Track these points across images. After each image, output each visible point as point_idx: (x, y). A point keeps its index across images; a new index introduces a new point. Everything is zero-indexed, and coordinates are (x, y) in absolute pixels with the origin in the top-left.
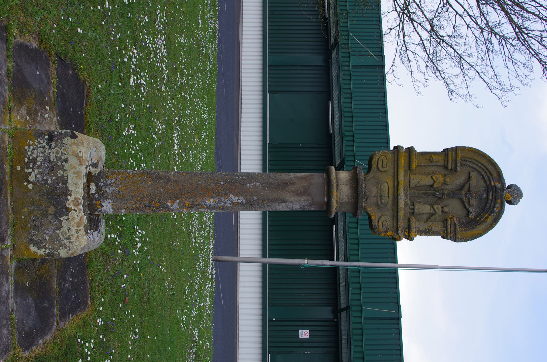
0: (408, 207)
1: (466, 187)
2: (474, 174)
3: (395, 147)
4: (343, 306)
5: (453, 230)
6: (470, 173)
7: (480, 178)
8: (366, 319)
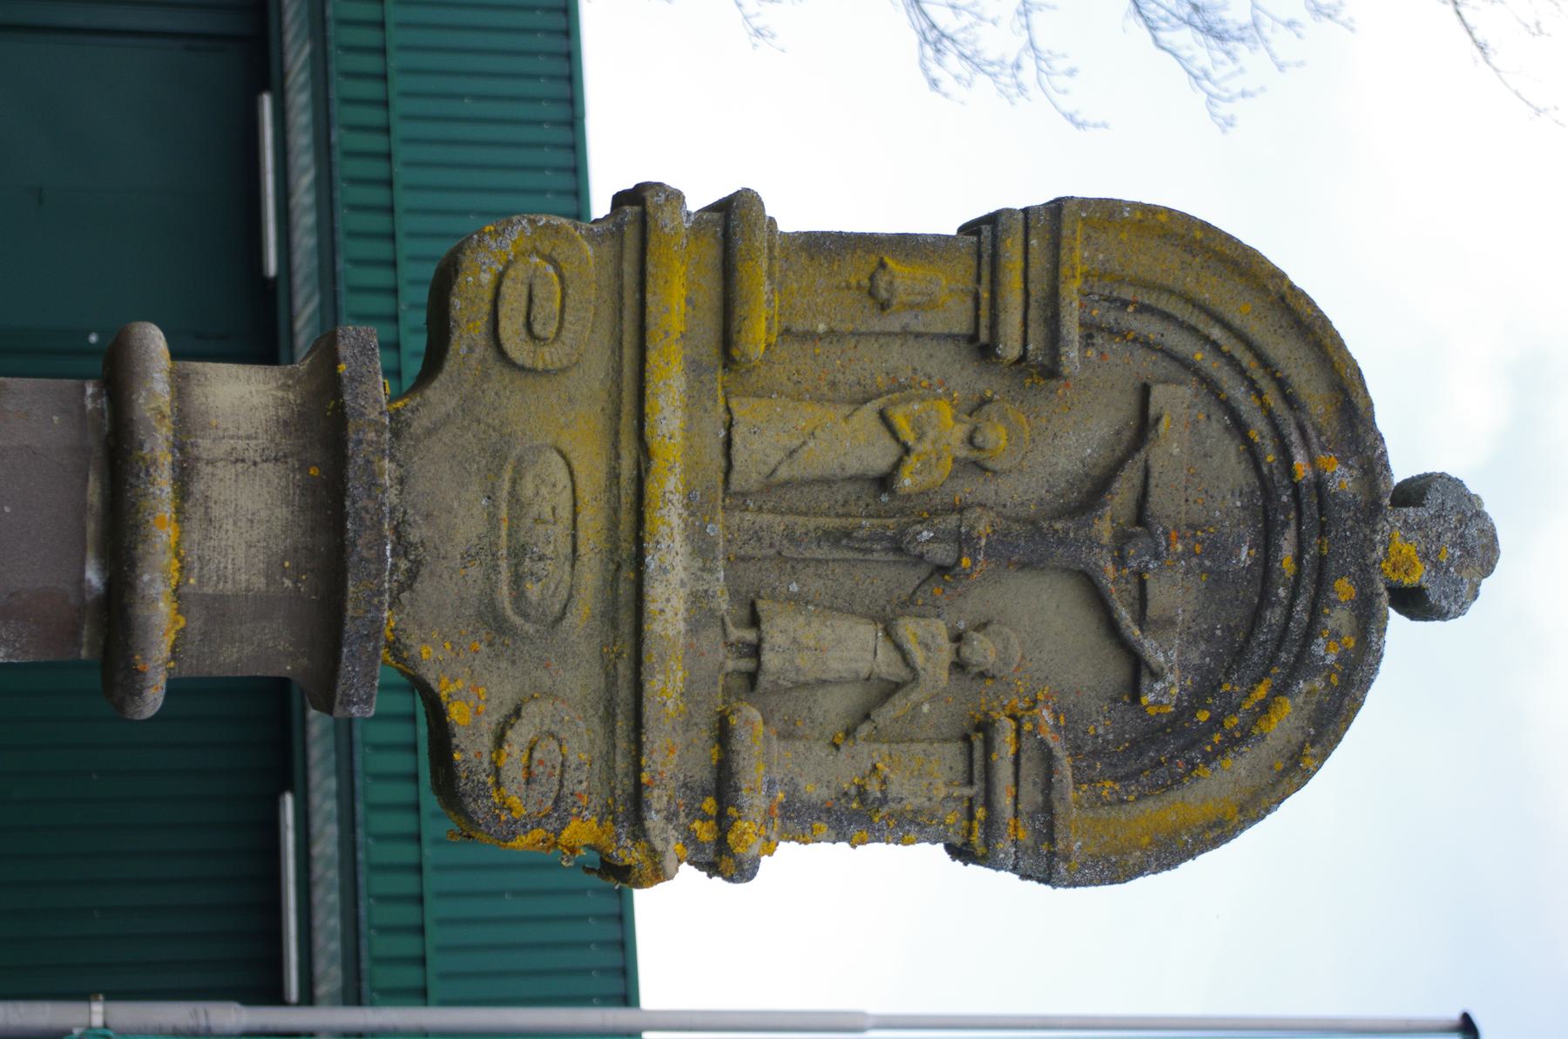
0: (714, 633)
1: (1122, 494)
5: (1031, 795)
6: (1145, 391)
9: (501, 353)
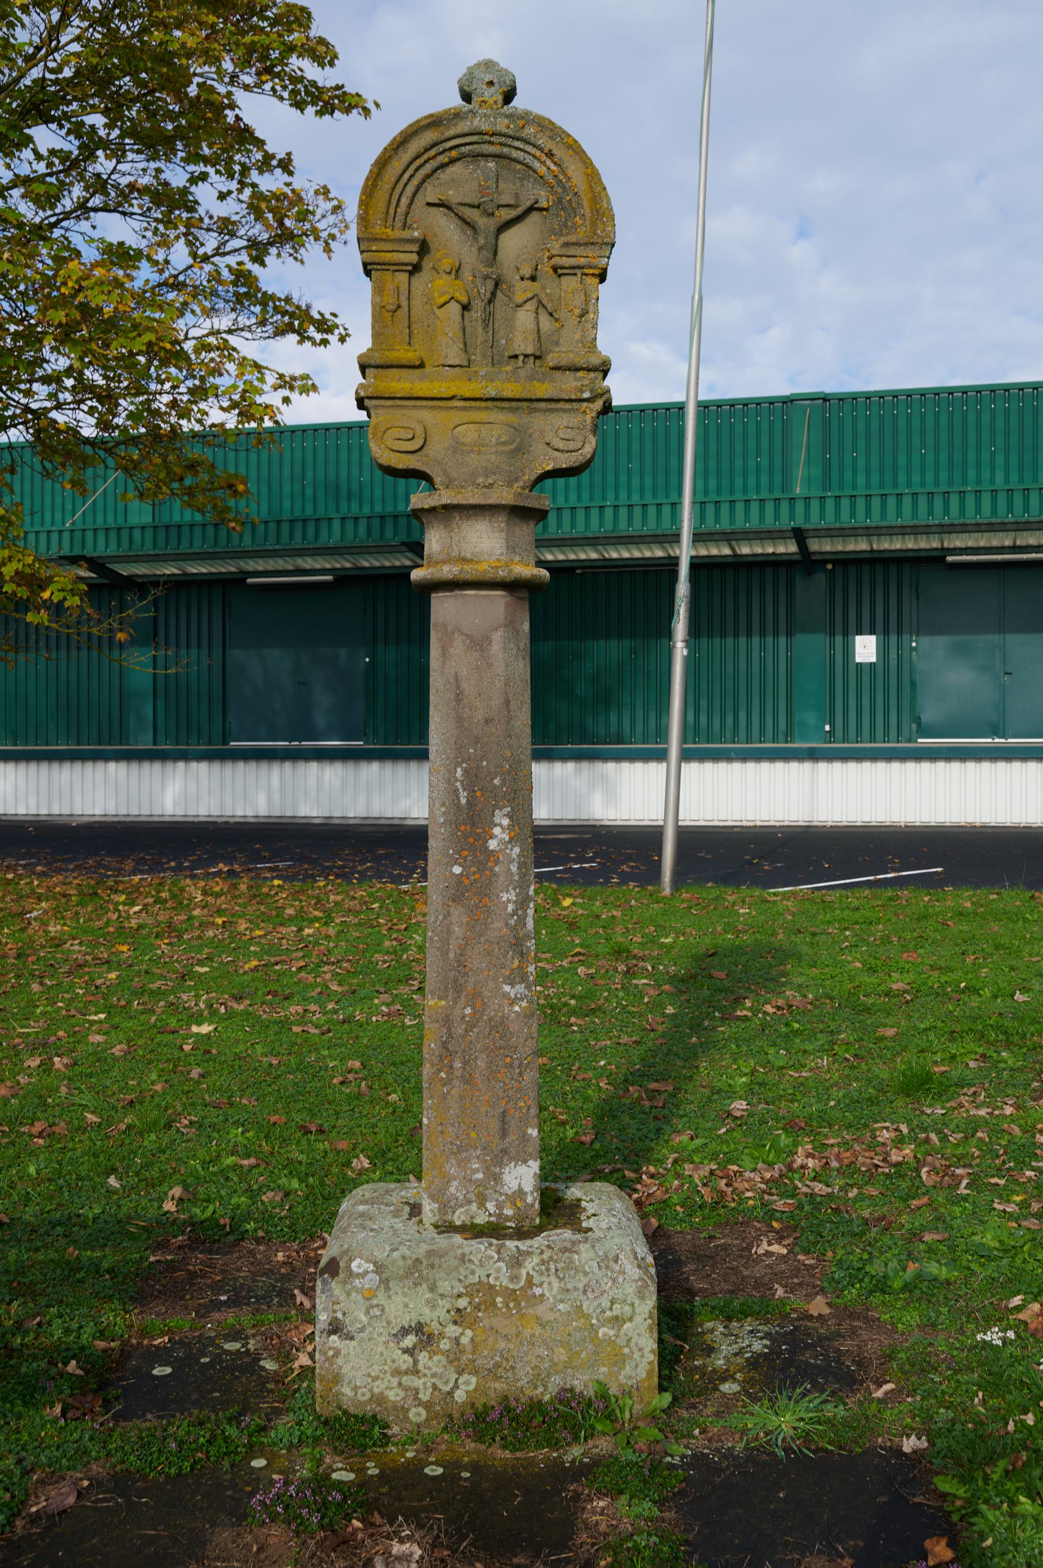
2: (431, 194)
3: (361, 404)
4: (790, 548)
6: (429, 204)
7: (444, 175)
8: (827, 485)
9: (420, 449)
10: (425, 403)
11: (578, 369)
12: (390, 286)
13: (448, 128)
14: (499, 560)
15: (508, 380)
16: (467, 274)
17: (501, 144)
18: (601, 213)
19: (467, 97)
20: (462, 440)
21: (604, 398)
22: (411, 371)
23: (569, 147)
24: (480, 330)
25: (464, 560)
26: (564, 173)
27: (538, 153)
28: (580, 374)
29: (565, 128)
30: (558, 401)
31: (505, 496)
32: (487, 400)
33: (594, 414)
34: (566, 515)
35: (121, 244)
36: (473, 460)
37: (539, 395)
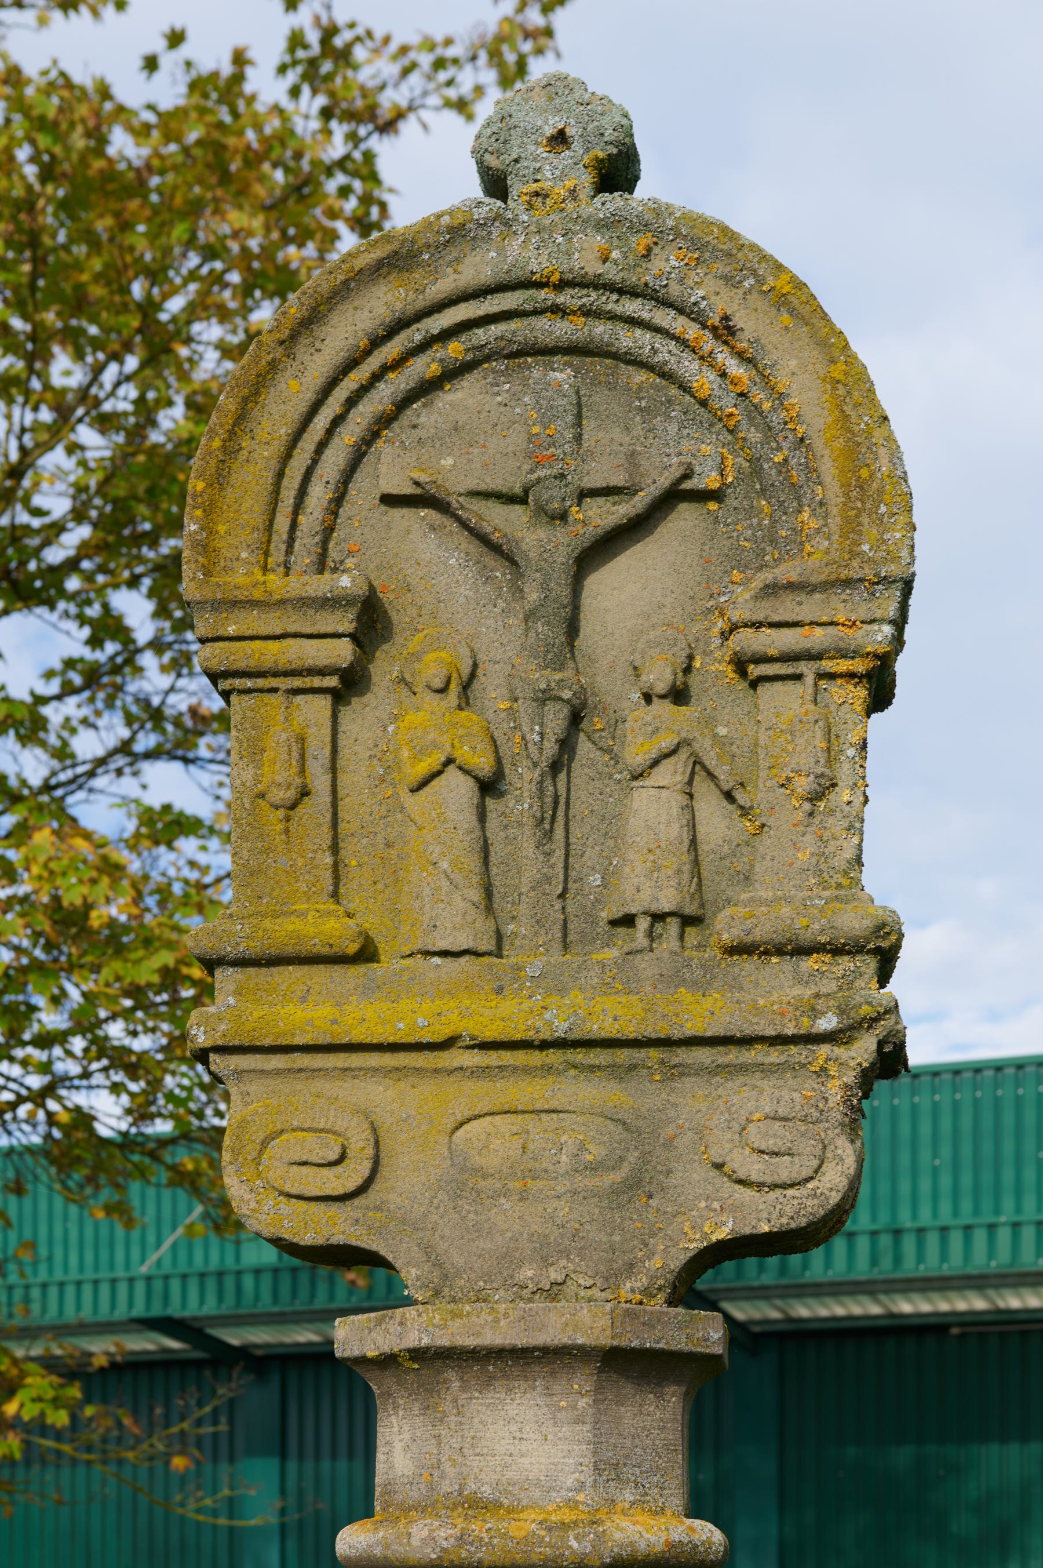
1: (498, 518)
2: (392, 468)
6: (390, 500)
9: (361, 1190)
10: (374, 1060)
11: (803, 951)
12: (279, 736)
13: (436, 275)
14: (572, 1504)
15: (606, 988)
16: (492, 690)
17: (587, 313)
18: (876, 489)
19: (496, 184)
20: (478, 1160)
21: (881, 1029)
22: (337, 972)
23: (781, 301)
24: (528, 848)
25: (476, 1505)
26: (765, 380)
27: (693, 331)
28: (810, 963)
29: (770, 248)
30: (747, 1041)
31: (587, 1323)
32: (544, 1045)
33: (850, 1077)
34: (932, 1240)
35: (167, 808)
36: (510, 1219)
37: (692, 1028)
